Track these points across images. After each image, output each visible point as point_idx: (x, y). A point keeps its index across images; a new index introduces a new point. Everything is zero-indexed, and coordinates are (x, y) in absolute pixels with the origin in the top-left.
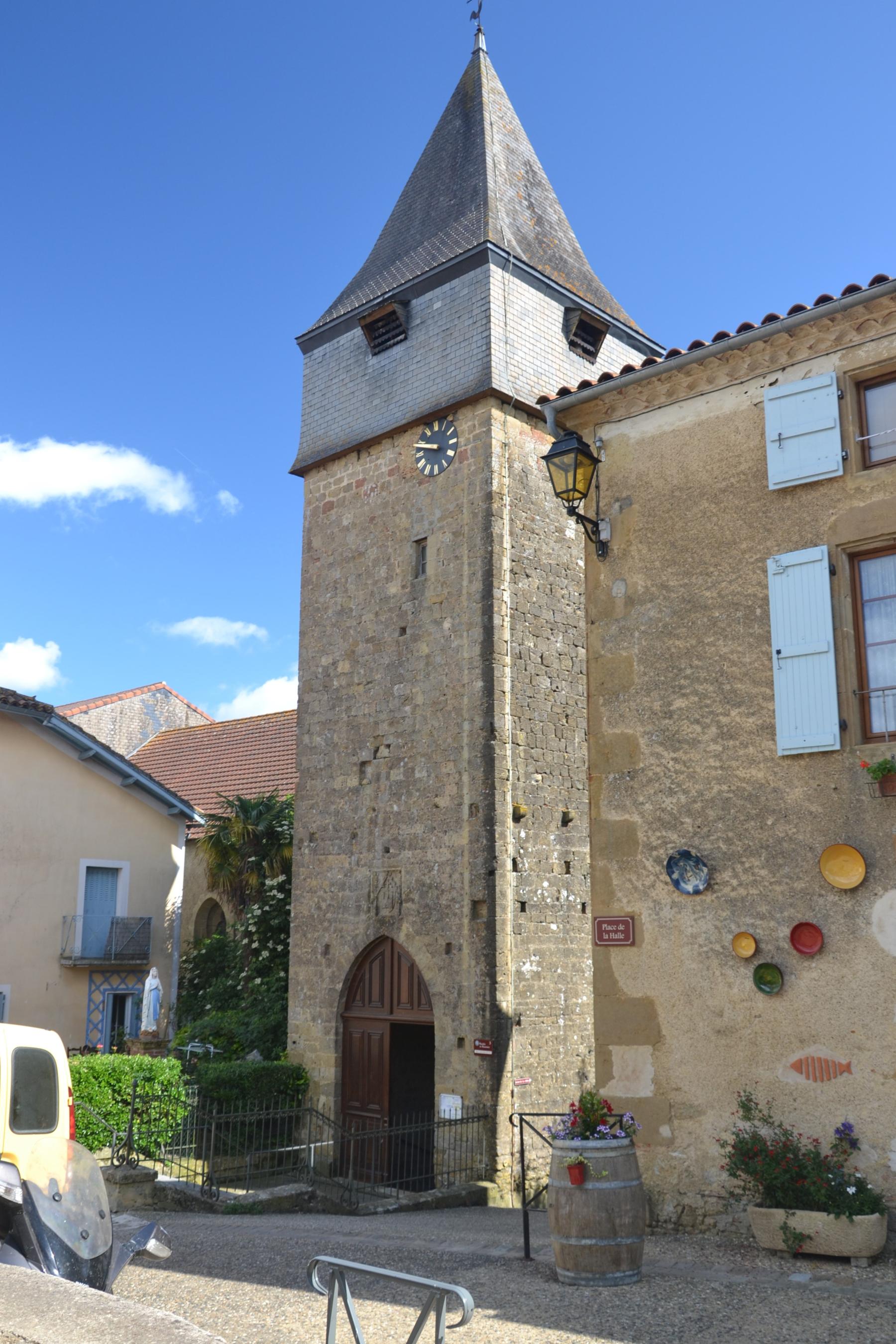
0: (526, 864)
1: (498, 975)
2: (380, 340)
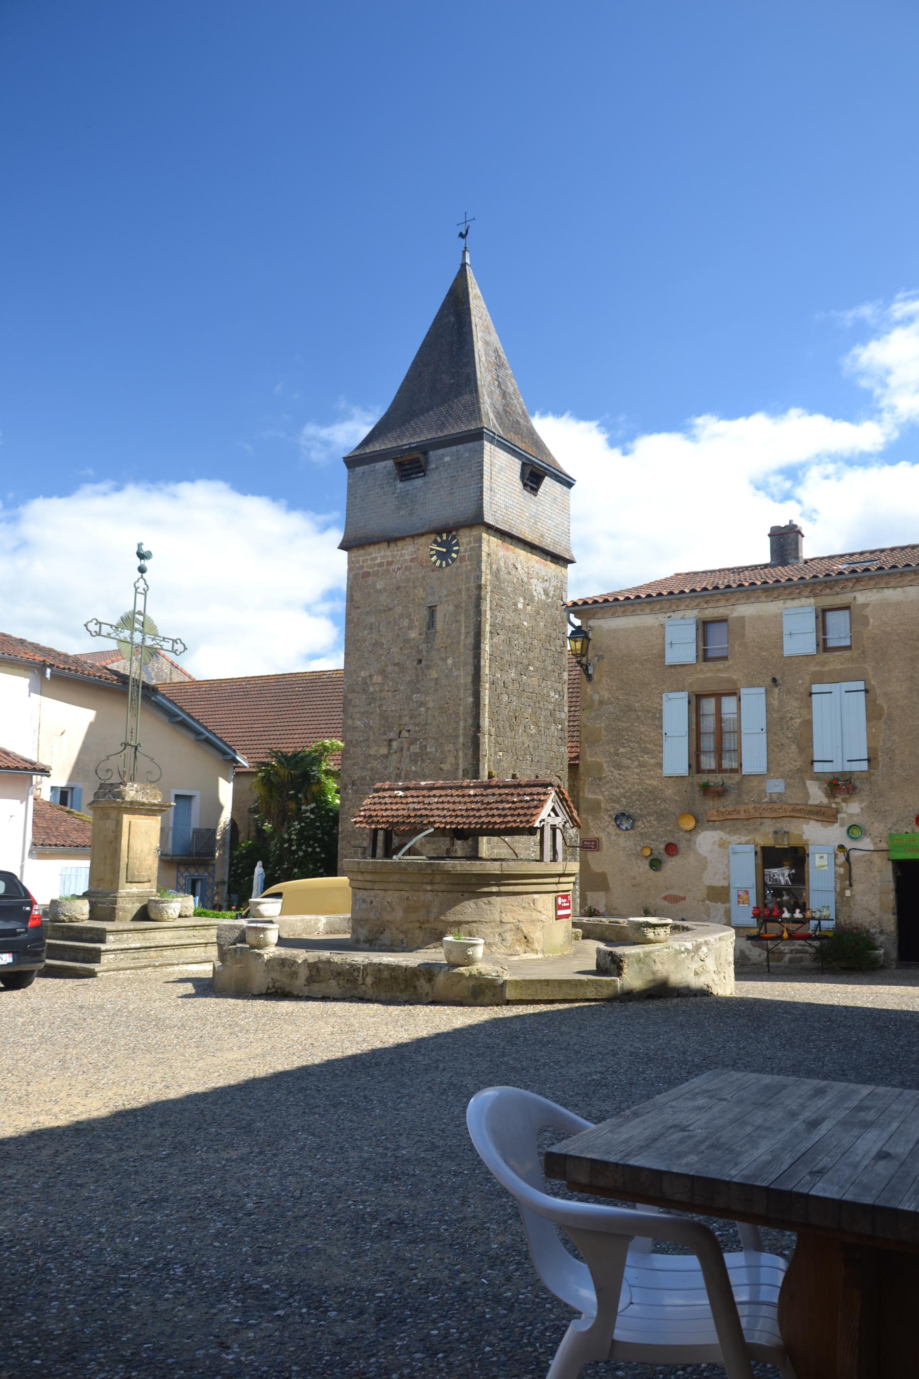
2: (406, 473)
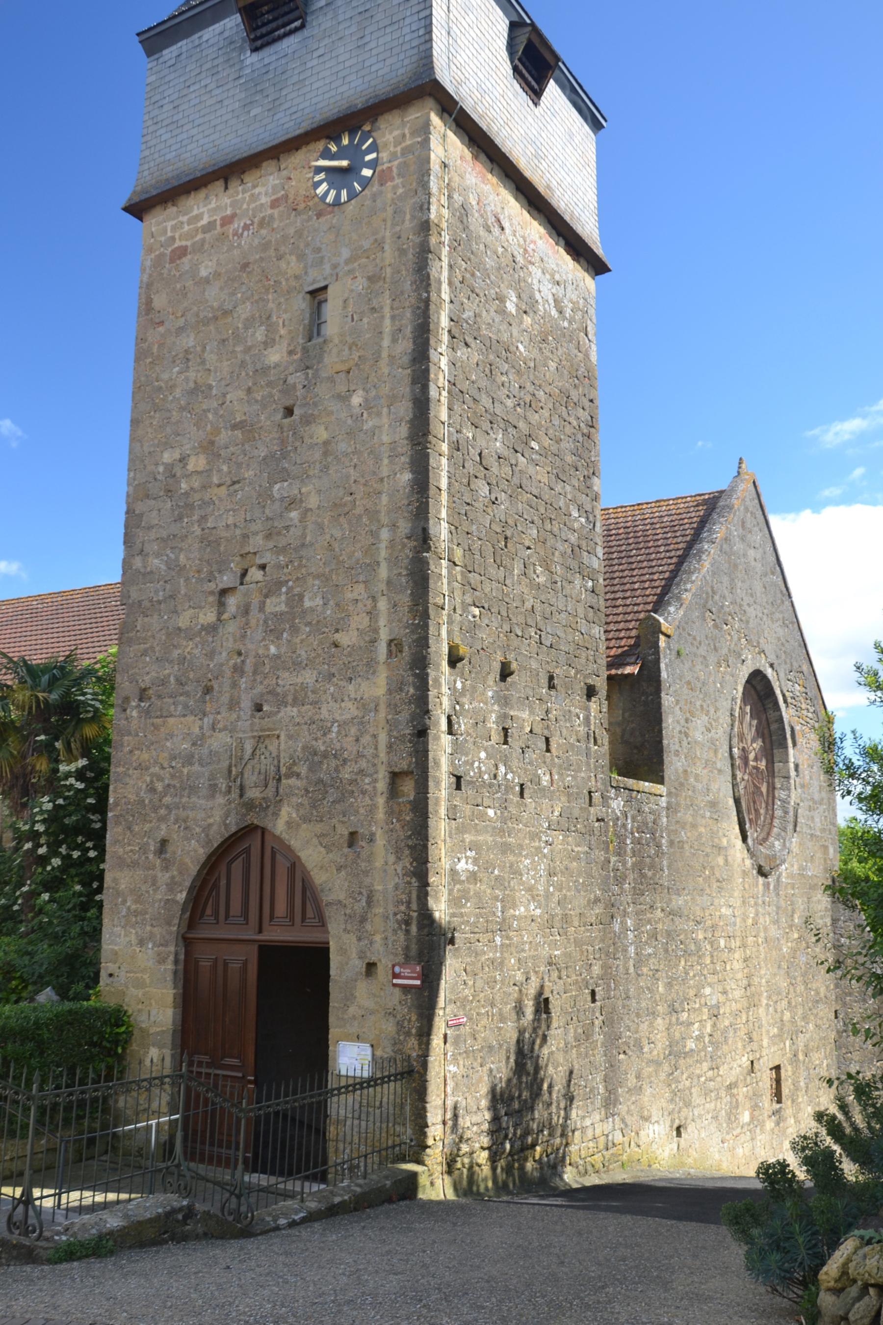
0: (463, 725)
1: (430, 874)
2: (264, 30)
